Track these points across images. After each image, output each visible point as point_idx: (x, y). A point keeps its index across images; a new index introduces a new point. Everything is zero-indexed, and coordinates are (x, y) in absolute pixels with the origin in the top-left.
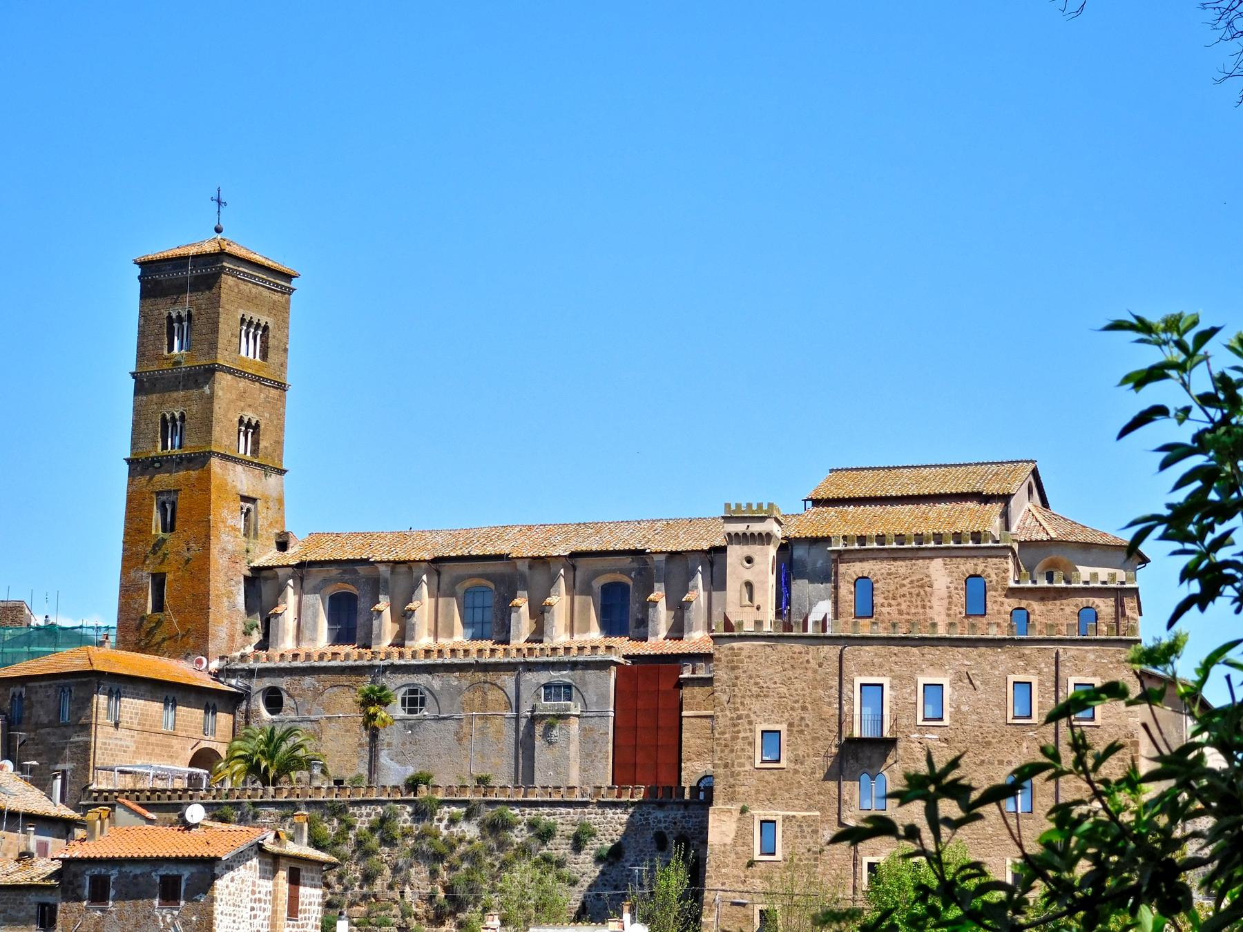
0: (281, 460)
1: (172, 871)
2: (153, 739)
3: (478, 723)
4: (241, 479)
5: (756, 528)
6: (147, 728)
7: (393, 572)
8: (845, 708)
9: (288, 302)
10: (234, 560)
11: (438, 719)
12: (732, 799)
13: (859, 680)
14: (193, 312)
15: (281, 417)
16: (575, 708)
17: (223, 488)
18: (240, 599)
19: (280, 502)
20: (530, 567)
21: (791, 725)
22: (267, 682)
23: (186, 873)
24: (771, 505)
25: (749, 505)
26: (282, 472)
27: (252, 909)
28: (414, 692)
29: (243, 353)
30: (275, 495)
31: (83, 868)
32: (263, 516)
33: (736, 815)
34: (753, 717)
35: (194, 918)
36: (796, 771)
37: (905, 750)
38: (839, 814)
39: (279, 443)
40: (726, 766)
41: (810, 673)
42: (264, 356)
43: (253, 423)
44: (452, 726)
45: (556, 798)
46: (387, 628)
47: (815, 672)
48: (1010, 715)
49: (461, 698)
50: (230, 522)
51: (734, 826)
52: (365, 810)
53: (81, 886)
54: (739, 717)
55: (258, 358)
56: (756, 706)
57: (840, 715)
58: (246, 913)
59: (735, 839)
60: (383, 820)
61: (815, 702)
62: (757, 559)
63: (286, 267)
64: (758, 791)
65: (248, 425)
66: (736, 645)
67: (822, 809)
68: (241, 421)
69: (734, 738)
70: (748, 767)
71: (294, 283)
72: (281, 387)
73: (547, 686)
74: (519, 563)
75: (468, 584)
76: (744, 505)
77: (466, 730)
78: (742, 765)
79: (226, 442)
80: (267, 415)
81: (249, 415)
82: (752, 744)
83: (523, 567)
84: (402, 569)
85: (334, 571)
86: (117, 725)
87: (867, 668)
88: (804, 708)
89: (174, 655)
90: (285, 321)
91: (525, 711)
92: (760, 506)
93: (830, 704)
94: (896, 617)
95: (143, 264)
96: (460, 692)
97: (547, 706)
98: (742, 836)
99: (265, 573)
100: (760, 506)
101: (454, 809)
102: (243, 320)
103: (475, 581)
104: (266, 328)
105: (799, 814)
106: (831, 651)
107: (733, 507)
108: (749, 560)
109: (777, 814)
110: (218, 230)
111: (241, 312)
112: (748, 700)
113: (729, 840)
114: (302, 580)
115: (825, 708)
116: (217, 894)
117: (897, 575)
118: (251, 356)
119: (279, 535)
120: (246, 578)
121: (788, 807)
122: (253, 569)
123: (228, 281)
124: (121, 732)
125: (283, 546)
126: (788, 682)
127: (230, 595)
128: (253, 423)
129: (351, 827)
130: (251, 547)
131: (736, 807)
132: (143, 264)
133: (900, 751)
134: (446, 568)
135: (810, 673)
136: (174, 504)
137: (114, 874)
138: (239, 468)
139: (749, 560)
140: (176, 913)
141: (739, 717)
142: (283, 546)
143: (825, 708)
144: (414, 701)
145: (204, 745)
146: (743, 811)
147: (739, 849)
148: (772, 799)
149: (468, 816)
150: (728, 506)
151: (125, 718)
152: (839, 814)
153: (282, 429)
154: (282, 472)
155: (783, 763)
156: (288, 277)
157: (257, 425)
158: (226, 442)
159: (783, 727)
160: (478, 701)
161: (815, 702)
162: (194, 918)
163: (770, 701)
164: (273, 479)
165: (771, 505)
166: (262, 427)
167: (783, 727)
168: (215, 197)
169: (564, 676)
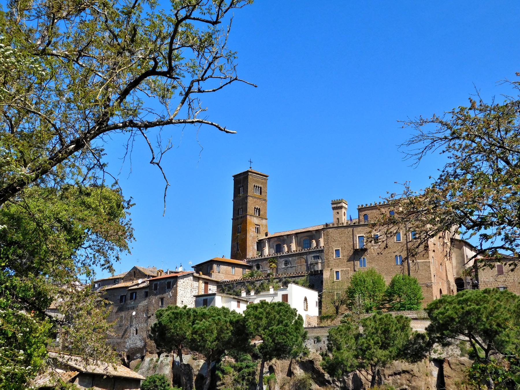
1: (169, 280)
2: (229, 276)
3: (299, 267)
4: (256, 220)
5: (339, 205)
7: (287, 237)
8: (355, 243)
9: (266, 182)
10: (253, 238)
11: (291, 267)
12: (329, 267)
13: (358, 236)
15: (266, 207)
16: (320, 261)
17: (251, 223)
18: (256, 247)
19: (266, 226)
20: (316, 233)
21: (342, 248)
23: (172, 280)
24: (342, 199)
26: (267, 219)
27: (191, 290)
28: (286, 261)
30: (265, 224)
32: (262, 229)
33: (330, 270)
34: (333, 247)
36: (344, 259)
37: (370, 251)
38: (354, 268)
39: (266, 213)
40: (327, 259)
41: (346, 235)
42: (261, 194)
44: (294, 268)
46: (286, 249)
47: (347, 234)
48: (395, 240)
49: (296, 261)
51: (329, 273)
52: (259, 282)
53: (152, 287)
54: (330, 247)
56: (334, 244)
57: (353, 244)
58: (189, 291)
59: (330, 277)
60: (262, 284)
61: (347, 242)
62: (340, 213)
63: (266, 174)
64: (335, 264)
65: (257, 209)
66: (328, 230)
67: (350, 268)
68: (255, 208)
69: (329, 252)
70: (332, 259)
72: (265, 200)
73: (314, 257)
74: (313, 232)
75: (304, 238)
77: (297, 269)
78: (330, 258)
79: (251, 212)
82: (333, 253)
83: (314, 233)
84: (289, 236)
85: (276, 239)
86: (219, 272)
87: (359, 232)
88: (345, 244)
89: (241, 260)
90: (266, 186)
91: (309, 263)
92: (339, 200)
93: (351, 242)
94: (58, 65)
95: (234, 176)
96: (296, 260)
97: (313, 261)
98: (331, 276)
99: (262, 241)
100: (339, 200)
101: (277, 280)
102: (254, 186)
103: (305, 237)
104: (261, 188)
105: (344, 269)
106: (350, 229)
108: (338, 213)
109: (339, 270)
110: (250, 168)
111: (254, 184)
112: (331, 243)
113: (328, 277)
114: (269, 242)
115: (350, 243)
116: (178, 285)
117: (373, 213)
119: (266, 233)
121: (342, 268)
122: (259, 240)
123: (250, 177)
124: (220, 274)
126: (341, 238)
127: (252, 246)
129: (255, 286)
130: (258, 235)
131: (329, 269)
132: (234, 176)
133: (368, 252)
134: (299, 235)
135: (346, 235)
137: (158, 283)
138: (255, 218)
139: (338, 213)
141: (330, 247)
142: (266, 235)
143: (350, 243)
144: (286, 263)
146: (331, 269)
147: (330, 279)
148: (338, 266)
149: (280, 281)
150: (332, 201)
151: (221, 271)
152: (354, 268)
153: (266, 210)
154: (267, 219)
155: (341, 257)
156: (267, 176)
158: (251, 212)
159: (340, 249)
160: (299, 262)
161: (347, 242)
163: (337, 242)
164: (264, 221)
165: (342, 199)
167: (340, 249)
168: (249, 160)
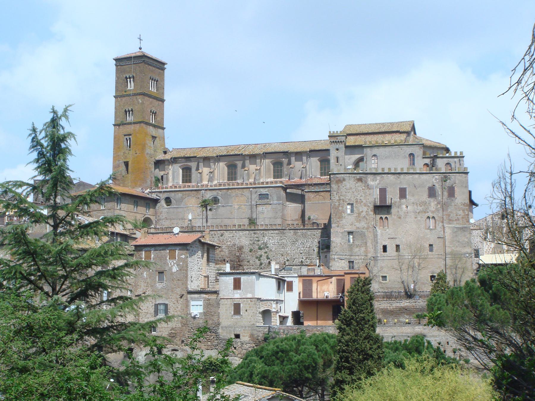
0: (163, 125)
6: (129, 210)
14: (134, 75)
22: (166, 195)
25: (334, 132)
27: (198, 261)
29: (151, 89)
31: (142, 248)
35: (181, 263)
43: (155, 112)
45: (274, 228)
50: (149, 145)
55: (155, 91)
68: (151, 111)
71: (166, 66)
76: (335, 132)
80: (159, 110)
81: (153, 109)
107: (332, 133)
118: (153, 90)
120: (154, 163)
125: (165, 153)
128: (155, 112)
136: (130, 139)
138: (151, 127)
140: (175, 262)
145: (146, 216)
150: (330, 132)
157: (156, 113)
162: (181, 263)
166: (157, 113)
169: (264, 191)
